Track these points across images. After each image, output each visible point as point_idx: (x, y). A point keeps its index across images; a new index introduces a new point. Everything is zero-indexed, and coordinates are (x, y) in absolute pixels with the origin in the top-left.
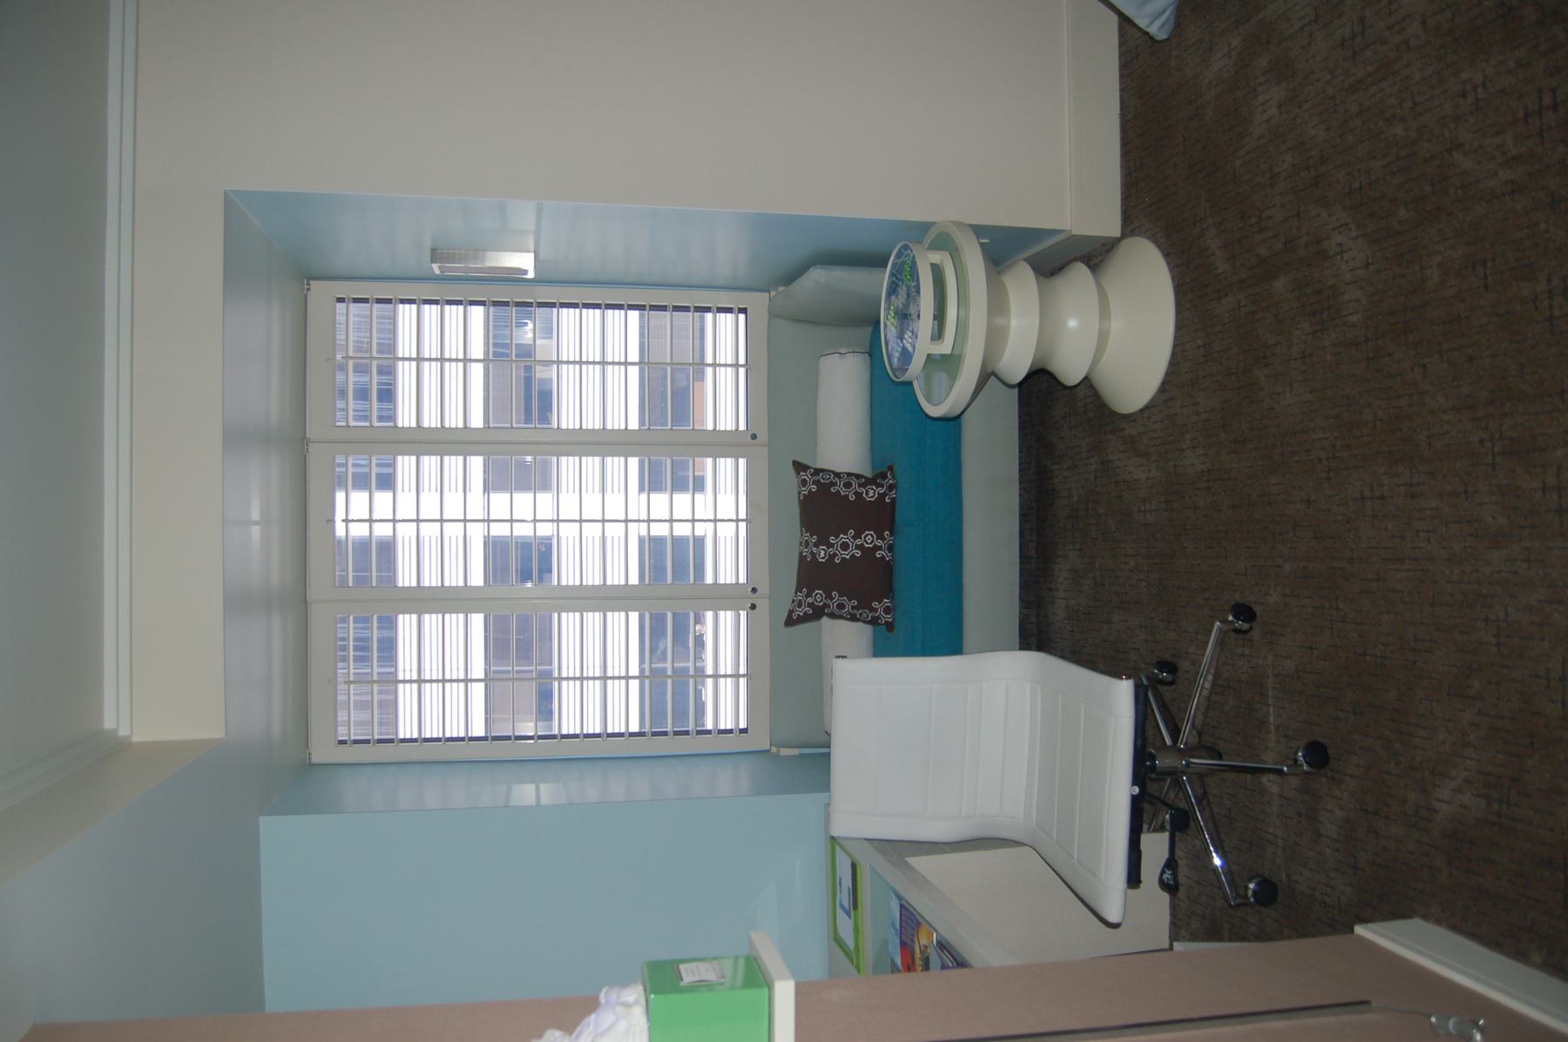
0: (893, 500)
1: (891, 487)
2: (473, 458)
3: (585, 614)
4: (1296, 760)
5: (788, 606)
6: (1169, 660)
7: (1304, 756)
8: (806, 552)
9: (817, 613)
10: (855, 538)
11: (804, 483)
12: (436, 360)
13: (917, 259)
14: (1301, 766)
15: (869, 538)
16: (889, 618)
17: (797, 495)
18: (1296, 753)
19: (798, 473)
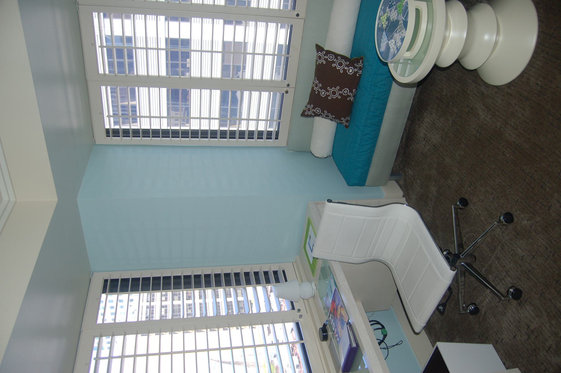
0: (360, 75)
1: (360, 68)
2: (163, 89)
3: (212, 90)
4: (500, 220)
5: (303, 108)
6: (466, 198)
7: (504, 219)
8: (315, 88)
9: (316, 115)
10: (339, 90)
11: (320, 58)
12: (139, 48)
13: (409, 6)
14: (503, 222)
15: (346, 91)
16: (347, 124)
17: (315, 62)
18: (500, 217)
19: (318, 52)
